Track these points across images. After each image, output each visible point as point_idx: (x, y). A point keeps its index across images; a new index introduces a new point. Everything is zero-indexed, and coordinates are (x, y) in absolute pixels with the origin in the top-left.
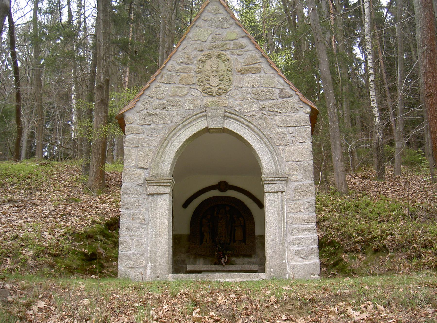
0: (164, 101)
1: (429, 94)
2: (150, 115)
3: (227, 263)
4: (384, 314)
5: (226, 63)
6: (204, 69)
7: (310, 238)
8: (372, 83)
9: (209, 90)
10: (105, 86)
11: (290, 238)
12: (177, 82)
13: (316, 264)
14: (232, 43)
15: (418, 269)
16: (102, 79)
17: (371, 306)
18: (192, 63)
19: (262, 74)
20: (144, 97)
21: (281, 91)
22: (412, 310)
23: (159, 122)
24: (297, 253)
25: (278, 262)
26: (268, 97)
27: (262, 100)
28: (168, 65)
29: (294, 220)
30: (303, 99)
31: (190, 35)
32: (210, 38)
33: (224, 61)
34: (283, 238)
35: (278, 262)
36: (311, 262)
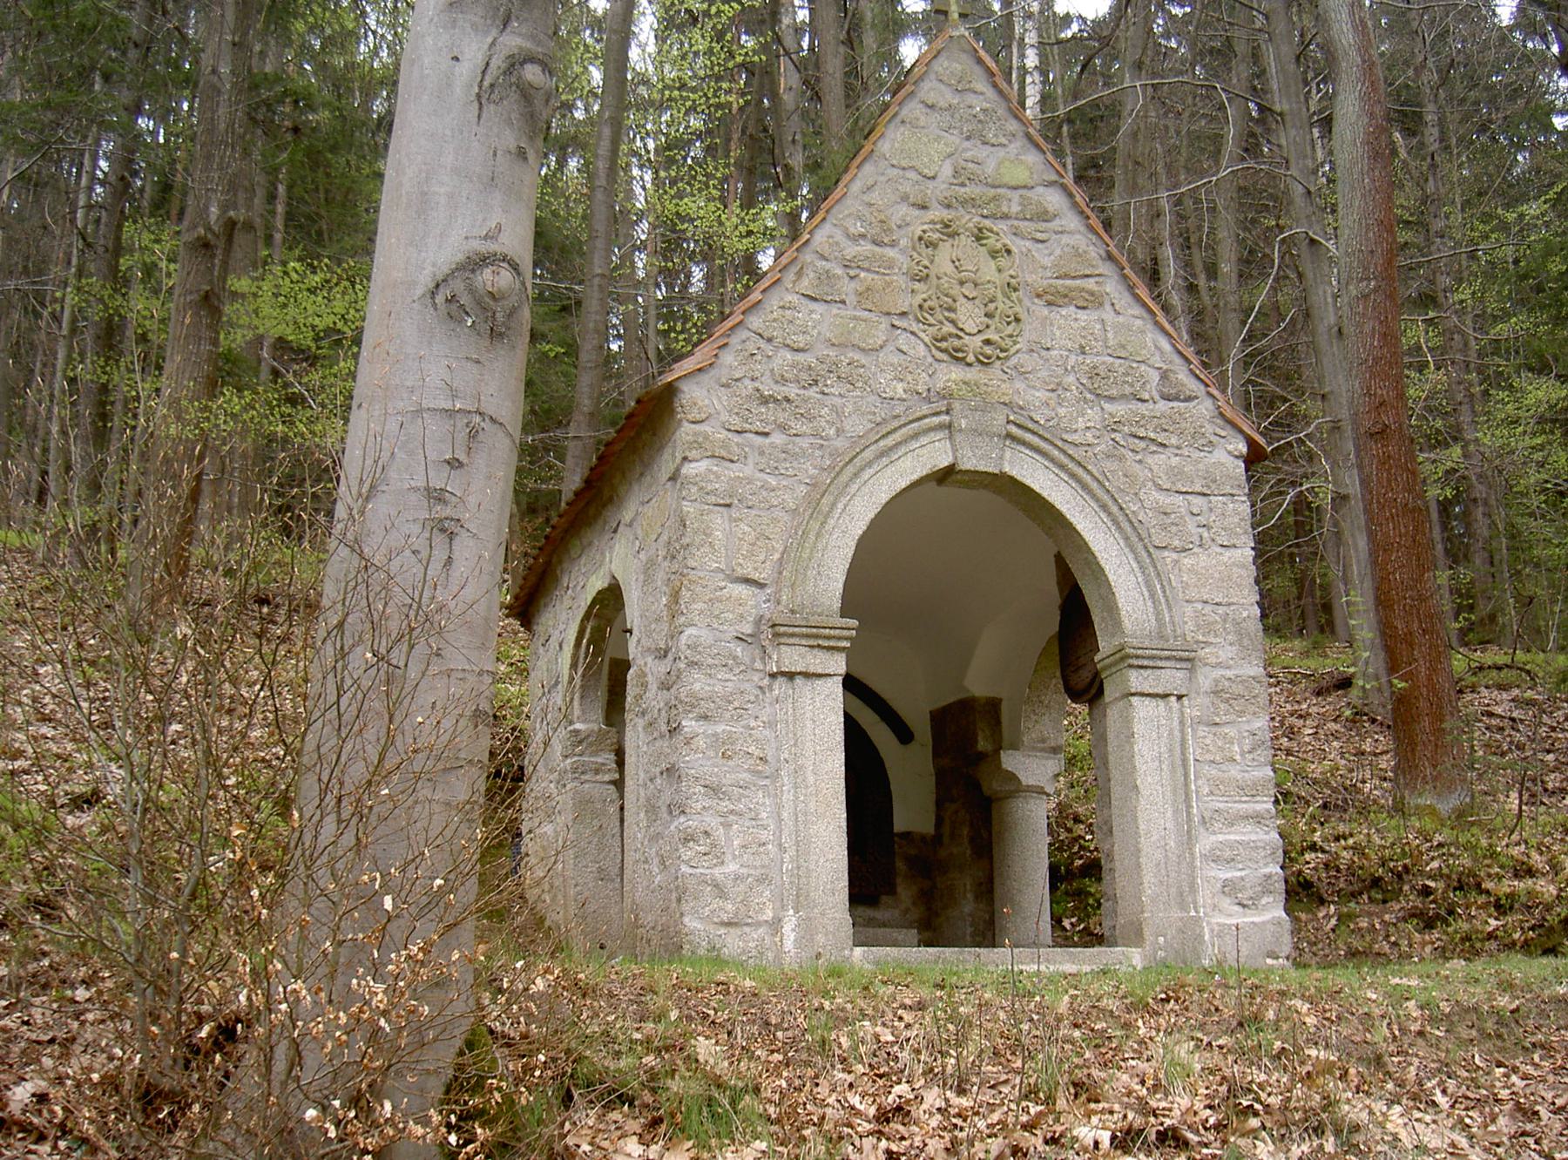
0: (809, 359)
2: (765, 400)
9: (957, 343)
12: (851, 300)
16: (213, 218)
18: (893, 244)
20: (743, 334)
21: (1164, 376)
24: (1229, 888)
26: (1128, 390)
27: (1111, 399)
32: (947, 170)
33: (994, 254)
34: (1189, 839)
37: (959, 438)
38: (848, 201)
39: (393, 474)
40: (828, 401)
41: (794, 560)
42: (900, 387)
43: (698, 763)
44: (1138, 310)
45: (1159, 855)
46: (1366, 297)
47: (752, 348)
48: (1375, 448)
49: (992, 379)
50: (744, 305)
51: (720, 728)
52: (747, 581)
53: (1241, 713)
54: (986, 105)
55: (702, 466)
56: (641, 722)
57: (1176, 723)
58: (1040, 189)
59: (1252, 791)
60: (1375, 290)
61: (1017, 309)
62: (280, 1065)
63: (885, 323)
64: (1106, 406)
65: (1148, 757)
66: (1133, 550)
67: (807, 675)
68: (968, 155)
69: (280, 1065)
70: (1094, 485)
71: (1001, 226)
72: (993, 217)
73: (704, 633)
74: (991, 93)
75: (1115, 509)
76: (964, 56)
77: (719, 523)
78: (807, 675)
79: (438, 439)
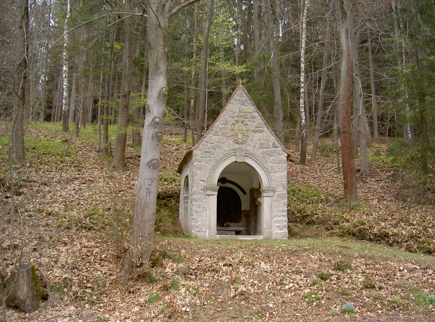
0: (214, 145)
1: (344, 131)
2: (206, 152)
3: (227, 226)
4: (323, 257)
5: (246, 126)
6: (235, 129)
7: (283, 220)
8: (302, 94)
9: (237, 141)
10: (128, 95)
11: (275, 219)
12: (221, 135)
13: (286, 232)
14: (249, 114)
15: (332, 235)
16: (126, 91)
17: (318, 254)
18: (228, 125)
19: (264, 134)
20: (203, 142)
21: (273, 143)
22: (334, 256)
23: (211, 156)
24: (278, 227)
25: (269, 231)
26: (267, 146)
27: (264, 148)
28: (216, 125)
29: (277, 210)
30: (284, 149)
31: (227, 108)
32: (238, 111)
33: (245, 125)
34: (272, 219)
35: (269, 231)
36: (284, 231)
41: (210, 177)
43: (195, 208)
45: (267, 221)
49: (243, 146)
61: (248, 134)
72: (245, 118)
74: (246, 96)
77: (199, 172)
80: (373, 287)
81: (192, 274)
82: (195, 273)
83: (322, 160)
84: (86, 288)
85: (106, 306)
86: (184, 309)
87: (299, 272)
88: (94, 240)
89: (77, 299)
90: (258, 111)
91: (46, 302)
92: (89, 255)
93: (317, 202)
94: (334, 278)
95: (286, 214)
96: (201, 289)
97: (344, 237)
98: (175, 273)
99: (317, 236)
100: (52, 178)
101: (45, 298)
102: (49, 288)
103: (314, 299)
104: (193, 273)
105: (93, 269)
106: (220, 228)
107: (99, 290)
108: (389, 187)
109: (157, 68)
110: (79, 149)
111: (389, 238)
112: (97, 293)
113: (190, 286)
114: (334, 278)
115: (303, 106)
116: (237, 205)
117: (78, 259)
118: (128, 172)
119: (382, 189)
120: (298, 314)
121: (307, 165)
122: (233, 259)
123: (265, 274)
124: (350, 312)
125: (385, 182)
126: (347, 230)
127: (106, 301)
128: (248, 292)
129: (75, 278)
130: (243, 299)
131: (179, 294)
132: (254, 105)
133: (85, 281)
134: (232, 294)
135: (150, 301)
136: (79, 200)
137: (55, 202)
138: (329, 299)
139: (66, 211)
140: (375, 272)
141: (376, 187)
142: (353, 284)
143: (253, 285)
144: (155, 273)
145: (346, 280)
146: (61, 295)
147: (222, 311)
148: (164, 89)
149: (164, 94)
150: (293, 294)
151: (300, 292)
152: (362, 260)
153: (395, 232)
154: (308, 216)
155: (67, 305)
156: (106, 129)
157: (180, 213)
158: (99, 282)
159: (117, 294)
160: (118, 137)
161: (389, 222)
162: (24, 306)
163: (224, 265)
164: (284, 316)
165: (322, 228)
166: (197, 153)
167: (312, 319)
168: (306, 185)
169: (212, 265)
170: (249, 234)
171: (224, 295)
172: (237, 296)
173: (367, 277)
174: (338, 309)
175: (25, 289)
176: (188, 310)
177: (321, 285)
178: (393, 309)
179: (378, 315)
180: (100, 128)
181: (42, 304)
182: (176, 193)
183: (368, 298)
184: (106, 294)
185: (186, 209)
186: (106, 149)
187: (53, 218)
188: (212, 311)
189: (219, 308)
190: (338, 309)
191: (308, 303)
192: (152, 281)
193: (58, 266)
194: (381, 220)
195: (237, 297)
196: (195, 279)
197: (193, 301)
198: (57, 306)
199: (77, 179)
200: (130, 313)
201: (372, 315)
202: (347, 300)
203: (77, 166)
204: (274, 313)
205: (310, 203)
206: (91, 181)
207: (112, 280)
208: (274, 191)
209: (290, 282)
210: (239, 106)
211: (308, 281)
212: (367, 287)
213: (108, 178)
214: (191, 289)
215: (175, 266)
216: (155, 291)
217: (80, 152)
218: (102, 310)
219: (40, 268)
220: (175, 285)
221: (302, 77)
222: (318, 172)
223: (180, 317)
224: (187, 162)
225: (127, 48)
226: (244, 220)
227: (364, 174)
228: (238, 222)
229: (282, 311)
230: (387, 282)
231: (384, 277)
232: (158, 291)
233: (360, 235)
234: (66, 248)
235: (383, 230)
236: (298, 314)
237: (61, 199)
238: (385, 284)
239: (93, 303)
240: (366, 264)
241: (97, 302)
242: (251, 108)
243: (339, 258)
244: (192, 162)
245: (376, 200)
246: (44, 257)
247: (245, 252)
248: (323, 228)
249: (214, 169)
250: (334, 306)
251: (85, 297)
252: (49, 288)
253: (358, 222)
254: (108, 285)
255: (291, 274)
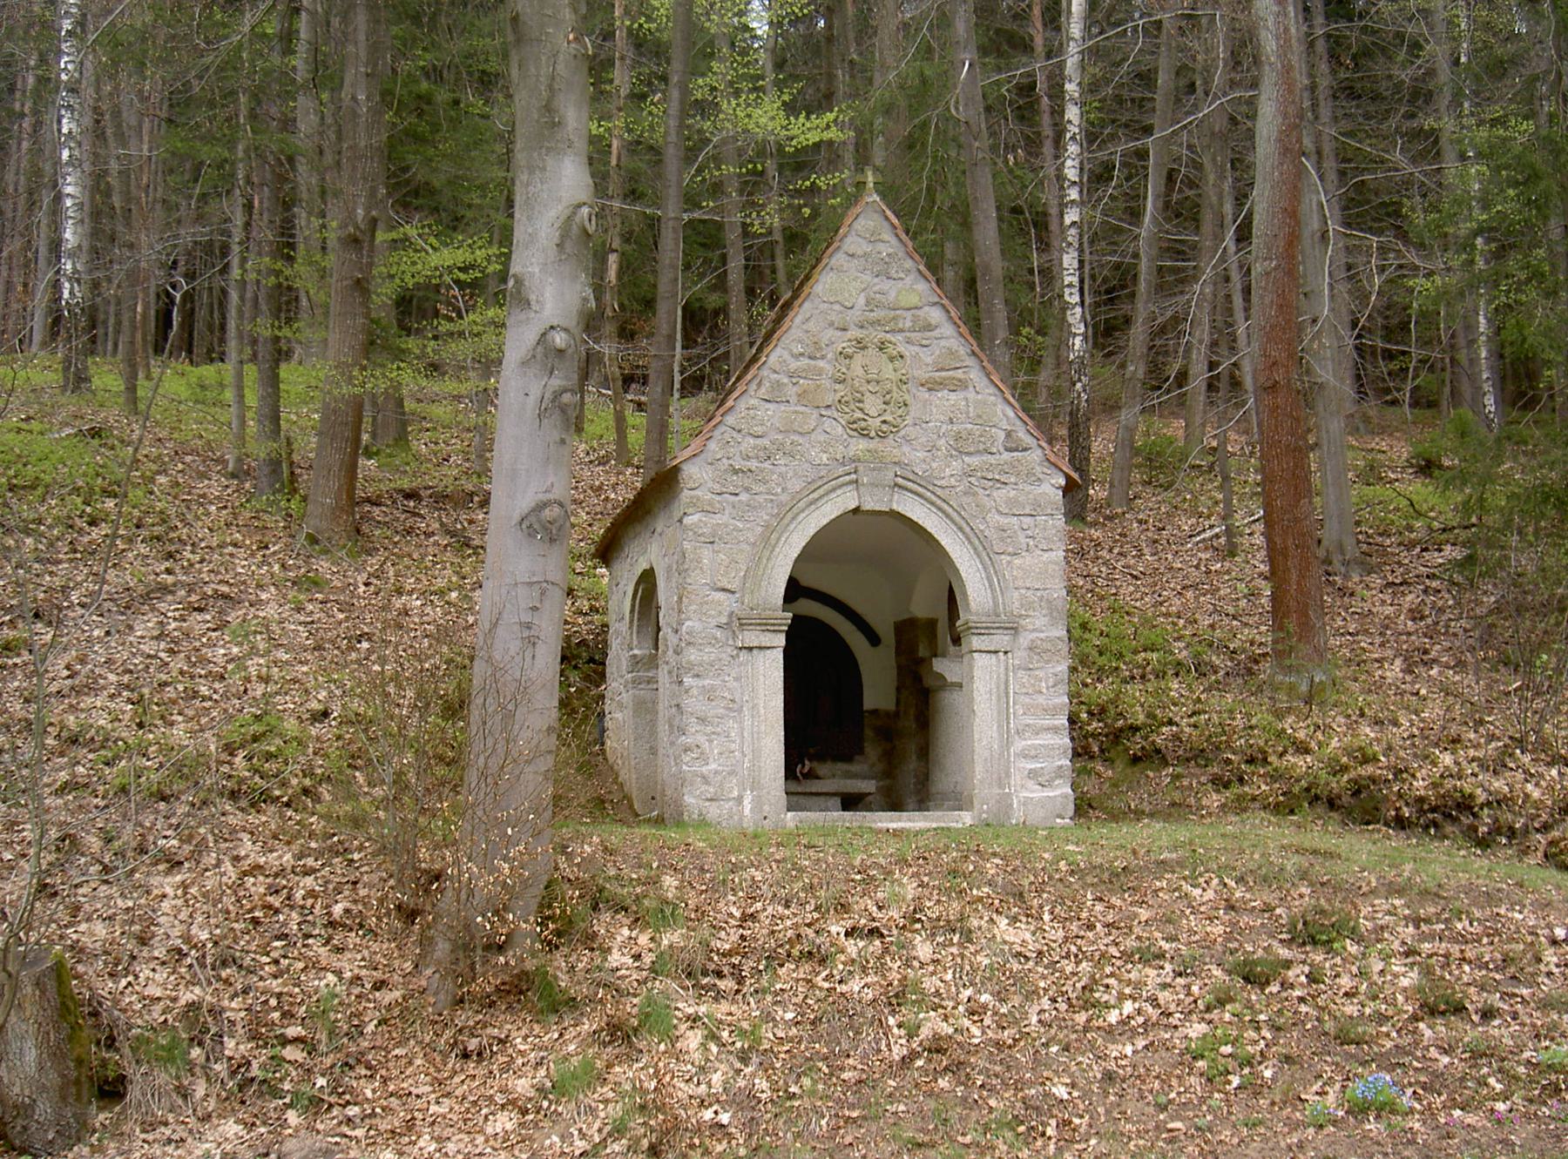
0: (765, 442)
2: (736, 472)
4: (1238, 894)
7: (1053, 744)
8: (1073, 231)
9: (863, 424)
12: (793, 400)
15: (1240, 806)
16: (360, 218)
17: (1216, 881)
18: (823, 357)
19: (971, 395)
20: (722, 428)
21: (1009, 434)
24: (1033, 774)
26: (981, 447)
27: (969, 454)
28: (773, 358)
32: (862, 301)
33: (892, 359)
34: (1009, 744)
37: (862, 489)
38: (793, 331)
39: (505, 616)
40: (777, 470)
41: (754, 573)
42: (825, 457)
43: (693, 703)
44: (992, 390)
45: (987, 754)
46: (1268, 274)
47: (727, 437)
48: (1268, 400)
49: (888, 448)
50: (721, 410)
51: (706, 682)
52: (724, 590)
53: (1048, 662)
54: (891, 250)
55: (695, 518)
56: (666, 668)
57: (1002, 670)
58: (927, 308)
59: (1053, 712)
60: (1275, 269)
61: (906, 397)
62: (463, 896)
63: (815, 414)
64: (966, 459)
65: (982, 690)
66: (979, 556)
67: (760, 648)
68: (876, 288)
69: (463, 896)
70: (954, 515)
71: (899, 337)
72: (892, 331)
73: (697, 624)
74: (894, 241)
75: (968, 530)
76: (876, 216)
77: (706, 554)
78: (760, 648)
79: (525, 597)
80: (1459, 1009)
81: (719, 974)
82: (734, 966)
83: (1151, 503)
84: (284, 1045)
85: (373, 1115)
86: (708, 1115)
87: (1153, 957)
88: (289, 843)
89: (246, 1089)
90: (945, 302)
91: (117, 1109)
92: (277, 904)
93: (1160, 675)
94: (1297, 974)
95: (1063, 721)
96: (767, 1032)
97: (1292, 812)
98: (652, 970)
99: (1176, 811)
100: (65, 589)
101: (111, 1090)
102: (127, 1051)
103: (1231, 1064)
104: (726, 970)
105: (301, 965)
106: (794, 787)
107: (338, 1049)
108: (1441, 610)
109: (551, 121)
110: (154, 467)
111: (1475, 815)
112: (328, 1061)
113: (721, 1022)
114: (1297, 974)
115: (1075, 280)
116: (862, 692)
117: (236, 925)
118: (371, 561)
119: (1413, 619)
120: (1178, 1125)
121: (1094, 524)
122: (880, 908)
123: (1016, 967)
124: (1385, 1109)
125: (1425, 591)
126: (1304, 783)
127: (369, 1094)
128: (959, 1038)
129: (233, 1005)
130: (946, 1069)
131: (678, 1056)
132: (927, 273)
133: (276, 1015)
134: (896, 1049)
135: (558, 1089)
136: (192, 677)
137: (91, 688)
138: (1288, 1059)
139: (141, 725)
140: (1455, 950)
141: (1389, 610)
142: (1375, 998)
143: (975, 1012)
144: (564, 969)
145: (1346, 982)
146: (178, 1078)
147: (864, 1118)
148: (585, 210)
149: (585, 231)
150: (1141, 1043)
151: (1167, 1036)
152: (1397, 902)
153: (1497, 792)
154: (1135, 729)
155: (206, 1118)
156: (272, 381)
157: (608, 723)
158: (332, 1016)
159: (410, 1063)
160: (328, 413)
161: (1472, 752)
162: (25, 1128)
163: (847, 934)
164: (1122, 1134)
165: (1196, 778)
166: (697, 476)
167: (1236, 1141)
168: (1105, 604)
169: (799, 936)
170: (895, 805)
171: (865, 1056)
172: (918, 1055)
173: (1427, 971)
174: (1331, 1098)
175: (31, 1055)
176: (725, 1118)
177: (1249, 1006)
178: (1551, 1097)
179: (1499, 1121)
180: (239, 376)
181: (101, 1117)
182: (583, 642)
183: (1446, 1052)
184: (369, 1067)
185: (645, 709)
186: (274, 464)
187: (91, 756)
188: (823, 1122)
189: (852, 1107)
190: (1331, 1098)
191: (1209, 1080)
192: (558, 1005)
193: (156, 954)
194: (1437, 745)
195: (920, 1063)
196: (738, 991)
197: (742, 1083)
198: (166, 1124)
199: (165, 589)
200: (480, 1139)
201: (1471, 1119)
202: (1364, 1064)
203: (158, 539)
204: (1076, 1121)
205: (1133, 678)
206: (225, 597)
207: (389, 1007)
208: (1015, 630)
209: (1121, 997)
210: (867, 277)
211: (1195, 989)
212: (1433, 1012)
213: (294, 583)
214: (725, 1034)
215: (644, 940)
216: (572, 1047)
217: (162, 479)
218: (359, 1133)
219: (80, 968)
220: (655, 1020)
221: (1069, 163)
222: (1146, 551)
223: (699, 1151)
224: (648, 512)
225: (362, 37)
226: (872, 751)
227: (1337, 560)
228: (848, 758)
229: (1108, 1112)
230: (1510, 990)
231: (1497, 969)
232: (584, 1044)
233: (1358, 803)
234: (179, 878)
235: (1449, 784)
236: (1178, 1125)
237: (112, 677)
238: (1501, 998)
239: (315, 1106)
240: (1417, 922)
241: (333, 1099)
242: (912, 289)
243: (1301, 896)
244: (677, 515)
245: (1398, 662)
246: (89, 920)
247: (926, 879)
248: (1203, 779)
249: (768, 540)
250: (1316, 1087)
251: (281, 1080)
252: (127, 1051)
253: (1348, 751)
254: (371, 1028)
255: (1118, 963)
